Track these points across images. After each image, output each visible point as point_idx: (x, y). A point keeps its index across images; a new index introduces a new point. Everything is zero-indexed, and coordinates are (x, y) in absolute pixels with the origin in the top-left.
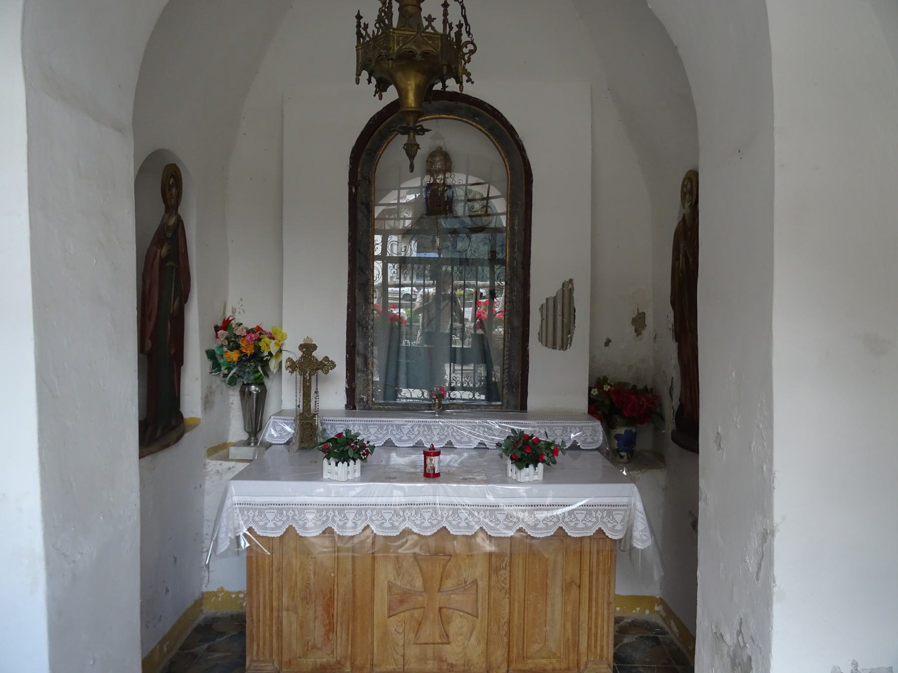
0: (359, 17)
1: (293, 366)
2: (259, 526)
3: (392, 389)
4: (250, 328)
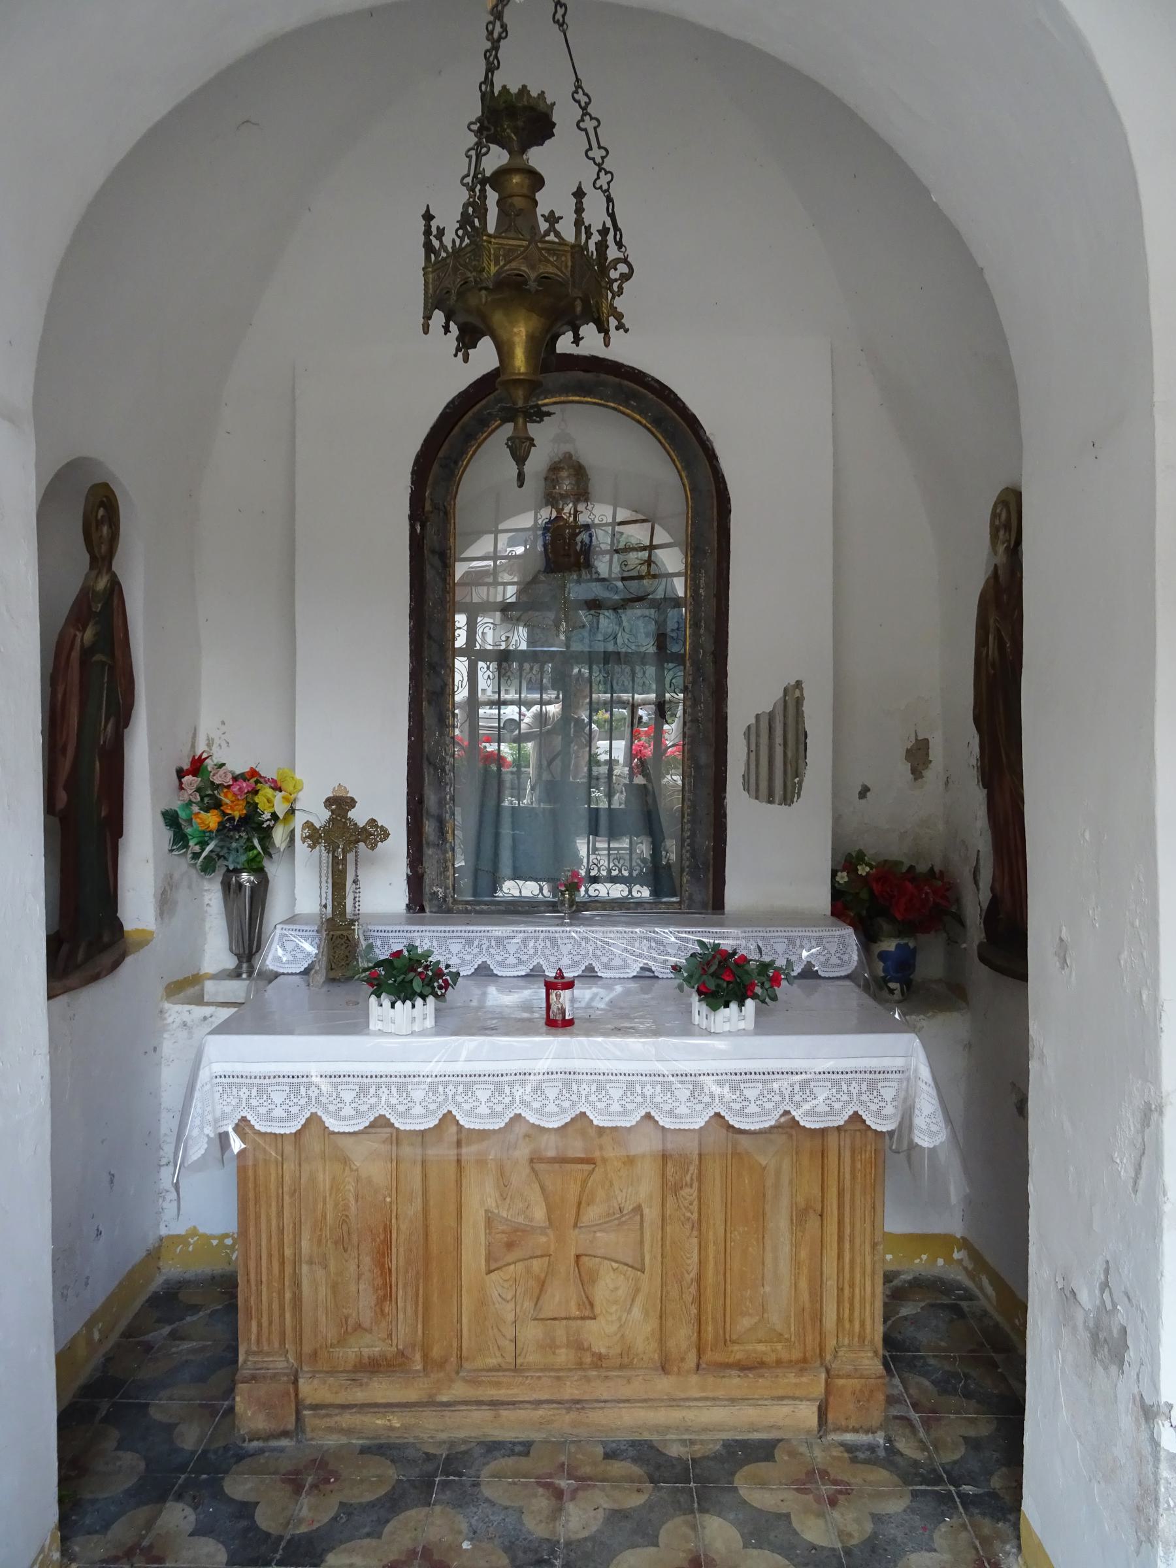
0: (428, 217)
1: (314, 836)
2: (258, 1115)
3: (487, 877)
4: (238, 772)
